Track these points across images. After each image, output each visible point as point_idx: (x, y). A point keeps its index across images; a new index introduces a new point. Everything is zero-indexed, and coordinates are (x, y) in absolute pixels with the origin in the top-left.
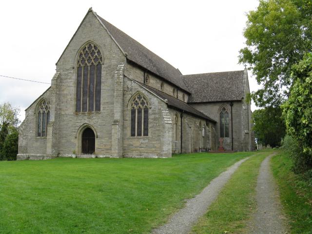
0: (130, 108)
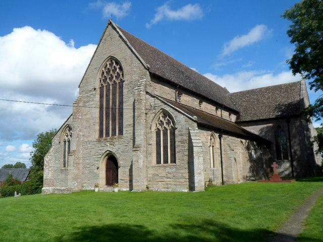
0: (154, 129)
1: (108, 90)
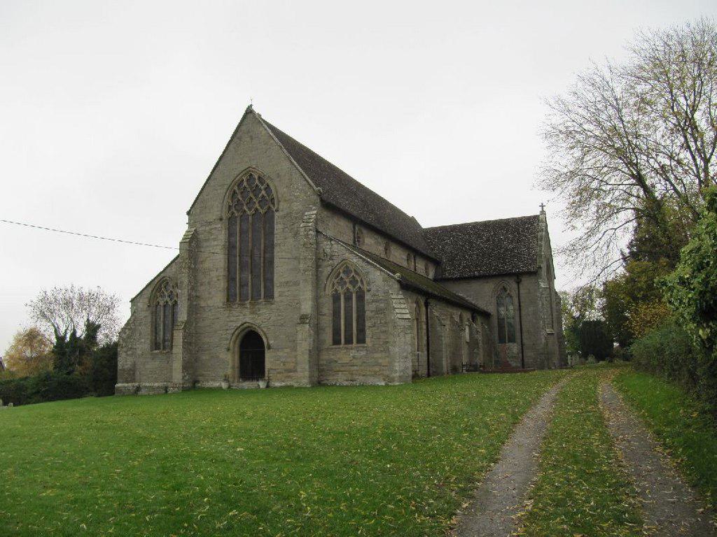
0: (329, 291)
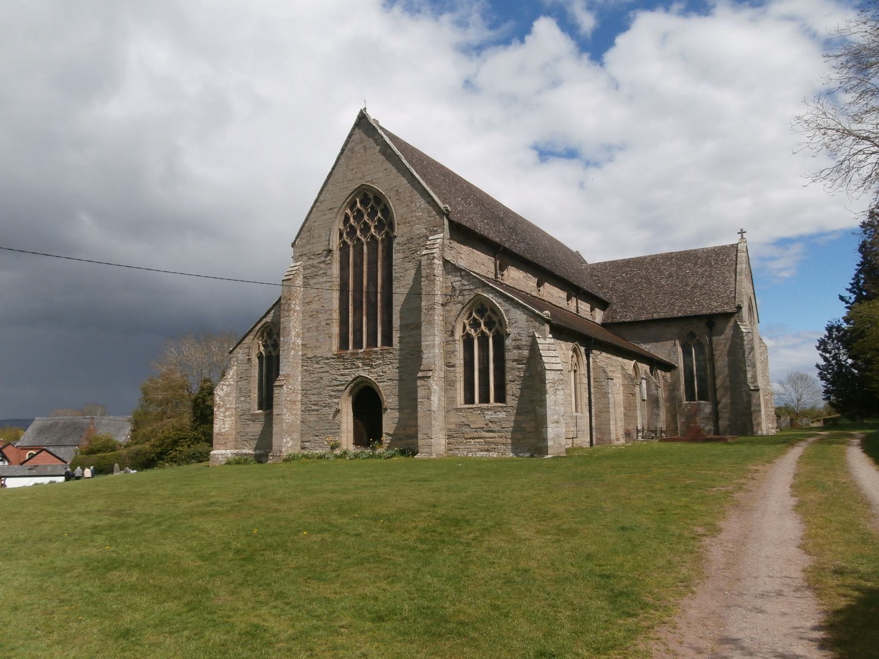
0: (459, 334)
1: (359, 254)
